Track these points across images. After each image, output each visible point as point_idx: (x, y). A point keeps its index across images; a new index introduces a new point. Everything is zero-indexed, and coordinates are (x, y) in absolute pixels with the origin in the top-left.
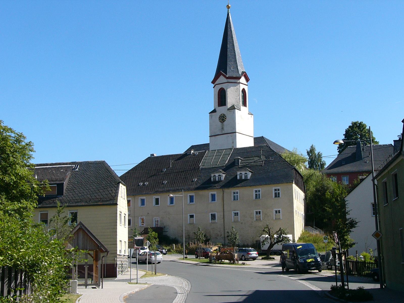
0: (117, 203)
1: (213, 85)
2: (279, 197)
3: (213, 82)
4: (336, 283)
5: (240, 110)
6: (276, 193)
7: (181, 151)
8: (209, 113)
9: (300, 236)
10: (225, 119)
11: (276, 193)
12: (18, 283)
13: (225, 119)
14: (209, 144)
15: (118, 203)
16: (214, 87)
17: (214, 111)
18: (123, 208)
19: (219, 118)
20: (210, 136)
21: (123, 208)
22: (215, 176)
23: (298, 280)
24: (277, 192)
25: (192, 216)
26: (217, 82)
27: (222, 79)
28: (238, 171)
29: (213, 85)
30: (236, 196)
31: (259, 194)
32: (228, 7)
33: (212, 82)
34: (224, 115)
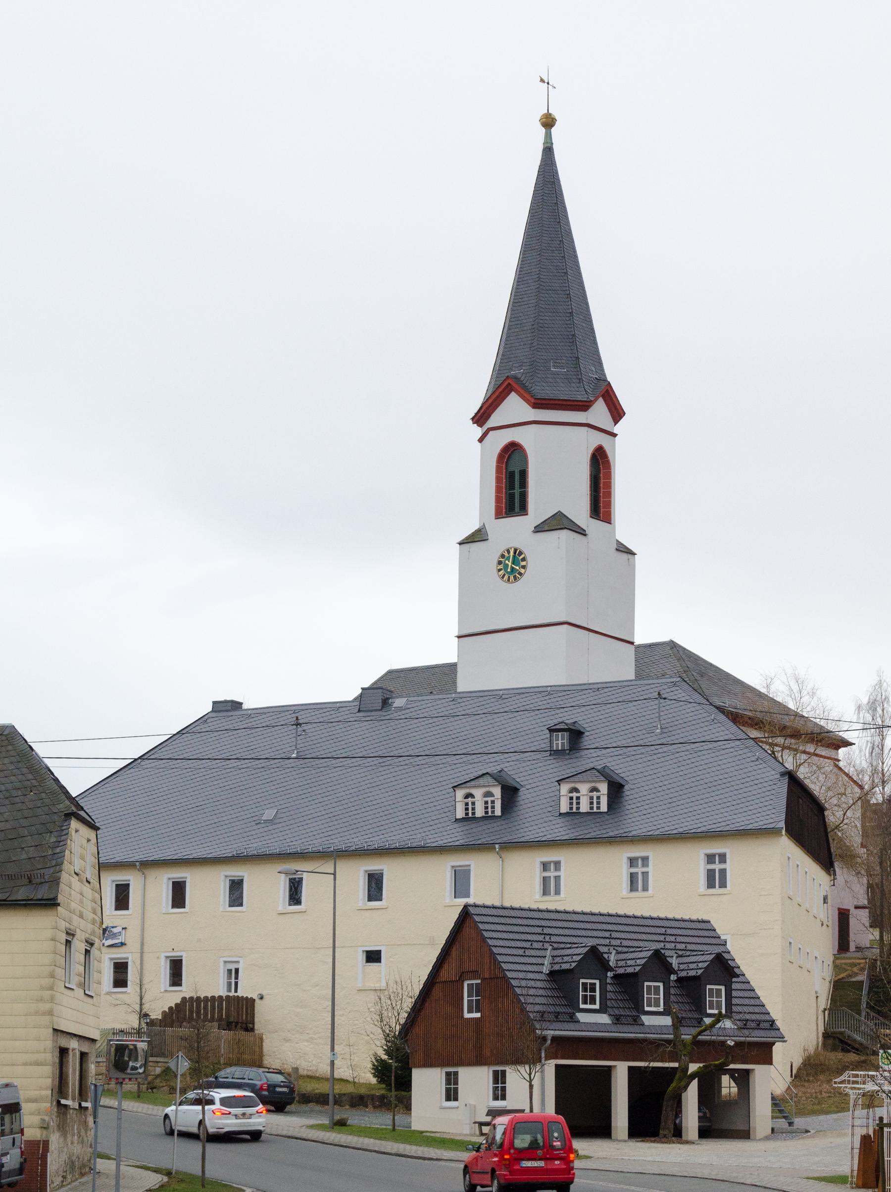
0: (55, 898)
1: (478, 431)
2: (723, 885)
3: (480, 418)
4: (207, 1175)
5: (585, 535)
6: (720, 862)
7: (341, 682)
8: (460, 544)
9: (812, 1050)
10: (522, 571)
11: (720, 862)
12: (496, 1182)
13: (522, 571)
14: (452, 667)
15: (60, 899)
16: (481, 440)
17: (477, 537)
18: (81, 916)
19: (500, 563)
20: (459, 637)
21: (81, 916)
22: (472, 796)
23: (138, 1167)
24: (717, 867)
25: (373, 957)
26: (495, 420)
27: (514, 408)
28: (463, 1016)
29: (478, 431)
30: (552, 879)
31: (643, 873)
32: (548, 122)
33: (473, 419)
34: (515, 578)
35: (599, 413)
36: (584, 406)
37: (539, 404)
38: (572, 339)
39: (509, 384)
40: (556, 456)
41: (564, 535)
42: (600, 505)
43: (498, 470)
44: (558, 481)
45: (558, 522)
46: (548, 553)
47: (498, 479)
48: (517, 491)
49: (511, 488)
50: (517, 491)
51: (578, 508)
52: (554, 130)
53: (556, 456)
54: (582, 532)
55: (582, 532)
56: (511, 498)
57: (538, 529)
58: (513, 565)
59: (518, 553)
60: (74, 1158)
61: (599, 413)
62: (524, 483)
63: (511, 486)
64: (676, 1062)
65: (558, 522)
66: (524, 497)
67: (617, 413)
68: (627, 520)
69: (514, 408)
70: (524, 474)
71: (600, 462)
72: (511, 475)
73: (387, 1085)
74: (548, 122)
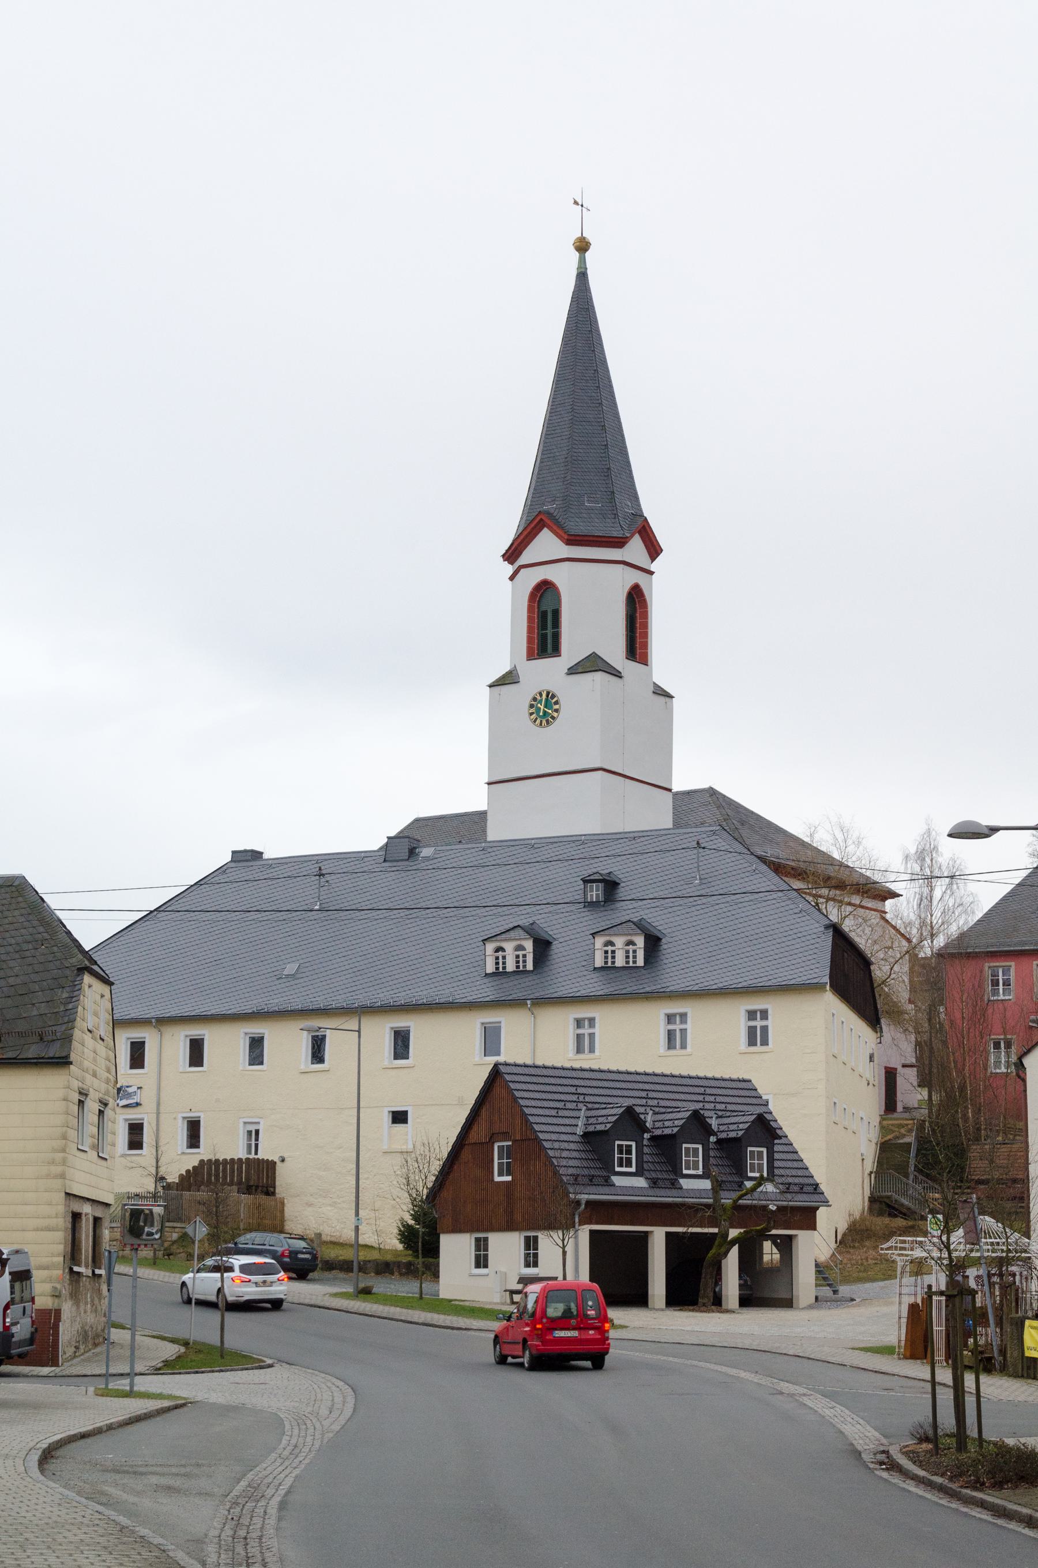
16: (512, 578)
32: (582, 246)
36: (619, 543)
37: (572, 540)
39: (541, 520)
40: (590, 597)
42: (637, 646)
43: (530, 609)
44: (591, 618)
45: (592, 664)
47: (530, 619)
48: (549, 631)
49: (544, 630)
50: (549, 631)
51: (615, 652)
52: (587, 254)
54: (618, 675)
55: (618, 675)
56: (543, 638)
57: (572, 671)
58: (545, 709)
59: (550, 696)
61: (635, 550)
63: (543, 625)
65: (592, 664)
67: (654, 550)
68: (665, 662)
69: (547, 544)
70: (556, 614)
71: (636, 602)
72: (543, 615)
74: (582, 246)
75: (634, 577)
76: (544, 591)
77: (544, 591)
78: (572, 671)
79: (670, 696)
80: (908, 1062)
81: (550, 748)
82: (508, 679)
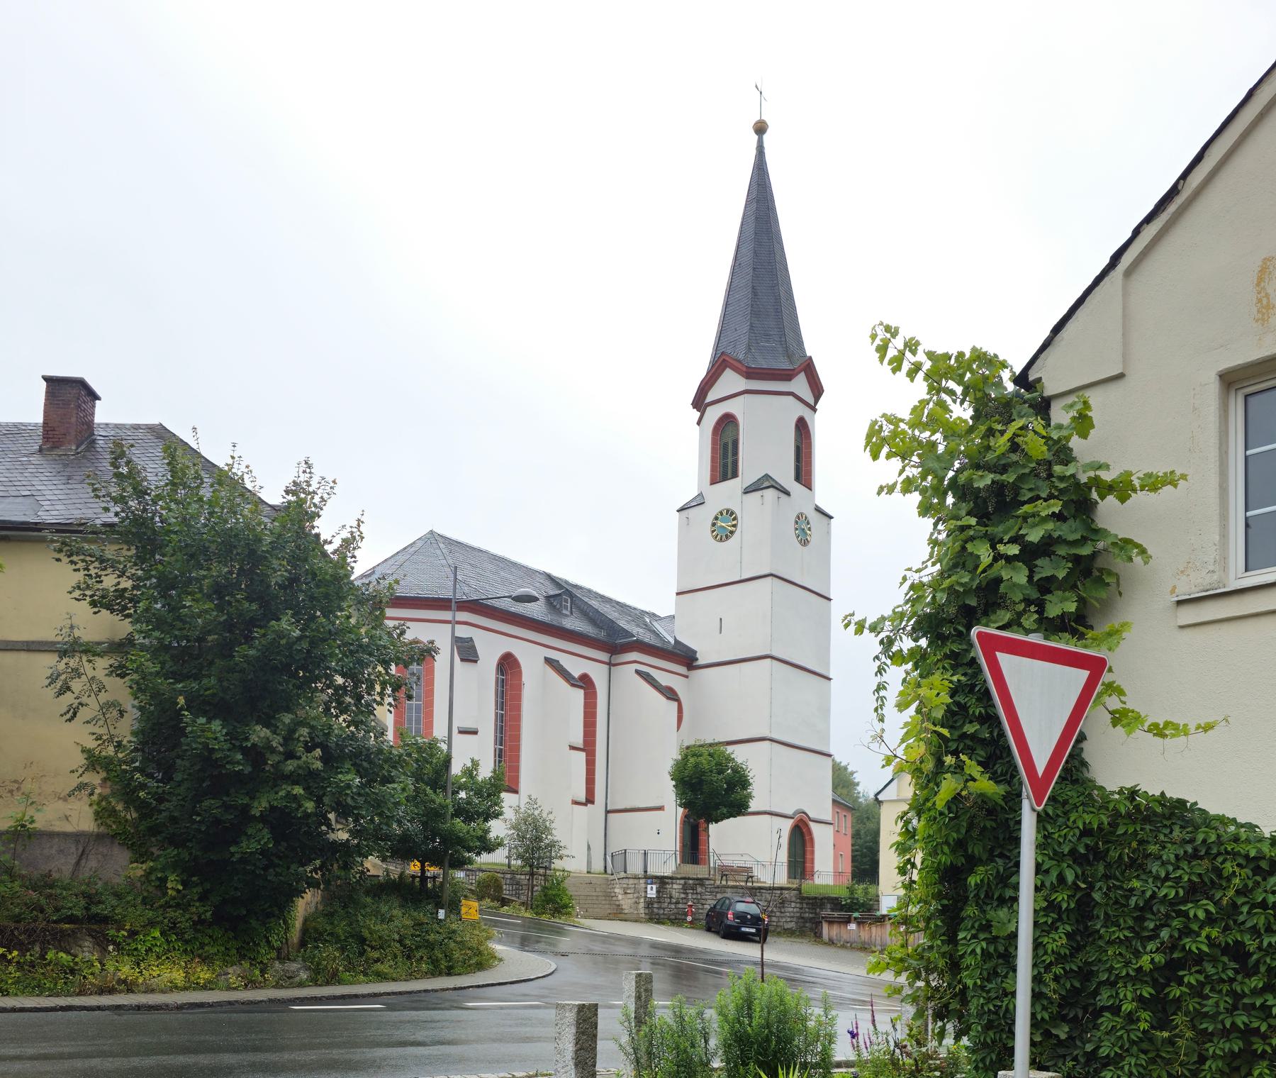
16: (699, 423)
32: (760, 129)
35: (800, 385)
36: (787, 376)
37: (750, 374)
38: (778, 311)
40: (764, 424)
41: (770, 494)
42: (803, 473)
43: (714, 442)
44: (764, 451)
45: (765, 483)
46: (758, 514)
47: (683, 831)
48: (730, 460)
49: (724, 459)
50: (730, 460)
51: (785, 475)
52: (765, 137)
53: (764, 424)
54: (787, 493)
55: (787, 493)
56: (725, 466)
57: (747, 491)
59: (730, 513)
60: (822, 1033)
61: (800, 385)
62: (735, 453)
63: (725, 456)
64: (300, 893)
65: (765, 483)
66: (735, 463)
67: (817, 390)
69: (731, 381)
71: (803, 430)
72: (725, 446)
73: (1079, 755)
74: (760, 129)
75: (802, 411)
76: (727, 424)
77: (727, 424)
78: (747, 491)
79: (831, 518)
80: (1114, 390)
81: (726, 560)
82: (699, 501)
